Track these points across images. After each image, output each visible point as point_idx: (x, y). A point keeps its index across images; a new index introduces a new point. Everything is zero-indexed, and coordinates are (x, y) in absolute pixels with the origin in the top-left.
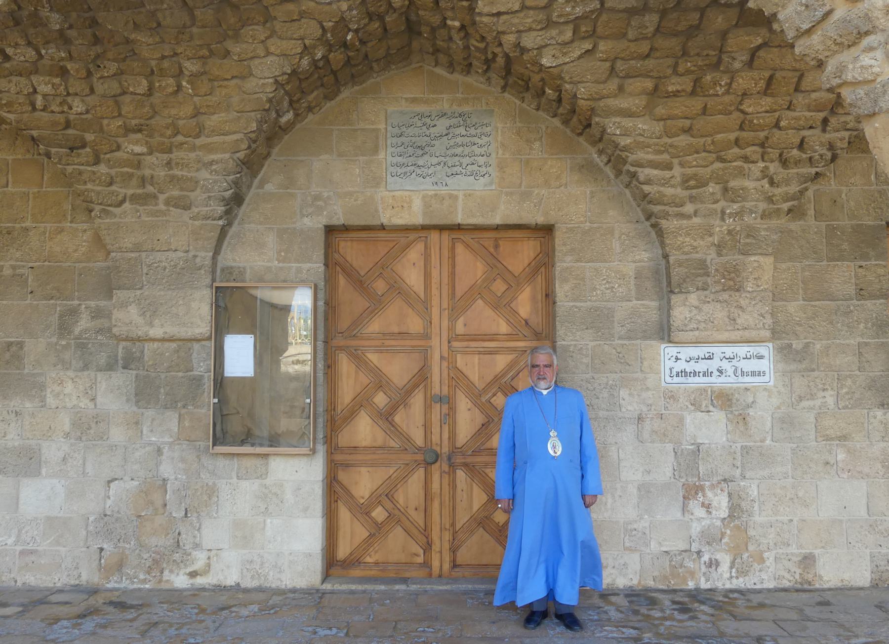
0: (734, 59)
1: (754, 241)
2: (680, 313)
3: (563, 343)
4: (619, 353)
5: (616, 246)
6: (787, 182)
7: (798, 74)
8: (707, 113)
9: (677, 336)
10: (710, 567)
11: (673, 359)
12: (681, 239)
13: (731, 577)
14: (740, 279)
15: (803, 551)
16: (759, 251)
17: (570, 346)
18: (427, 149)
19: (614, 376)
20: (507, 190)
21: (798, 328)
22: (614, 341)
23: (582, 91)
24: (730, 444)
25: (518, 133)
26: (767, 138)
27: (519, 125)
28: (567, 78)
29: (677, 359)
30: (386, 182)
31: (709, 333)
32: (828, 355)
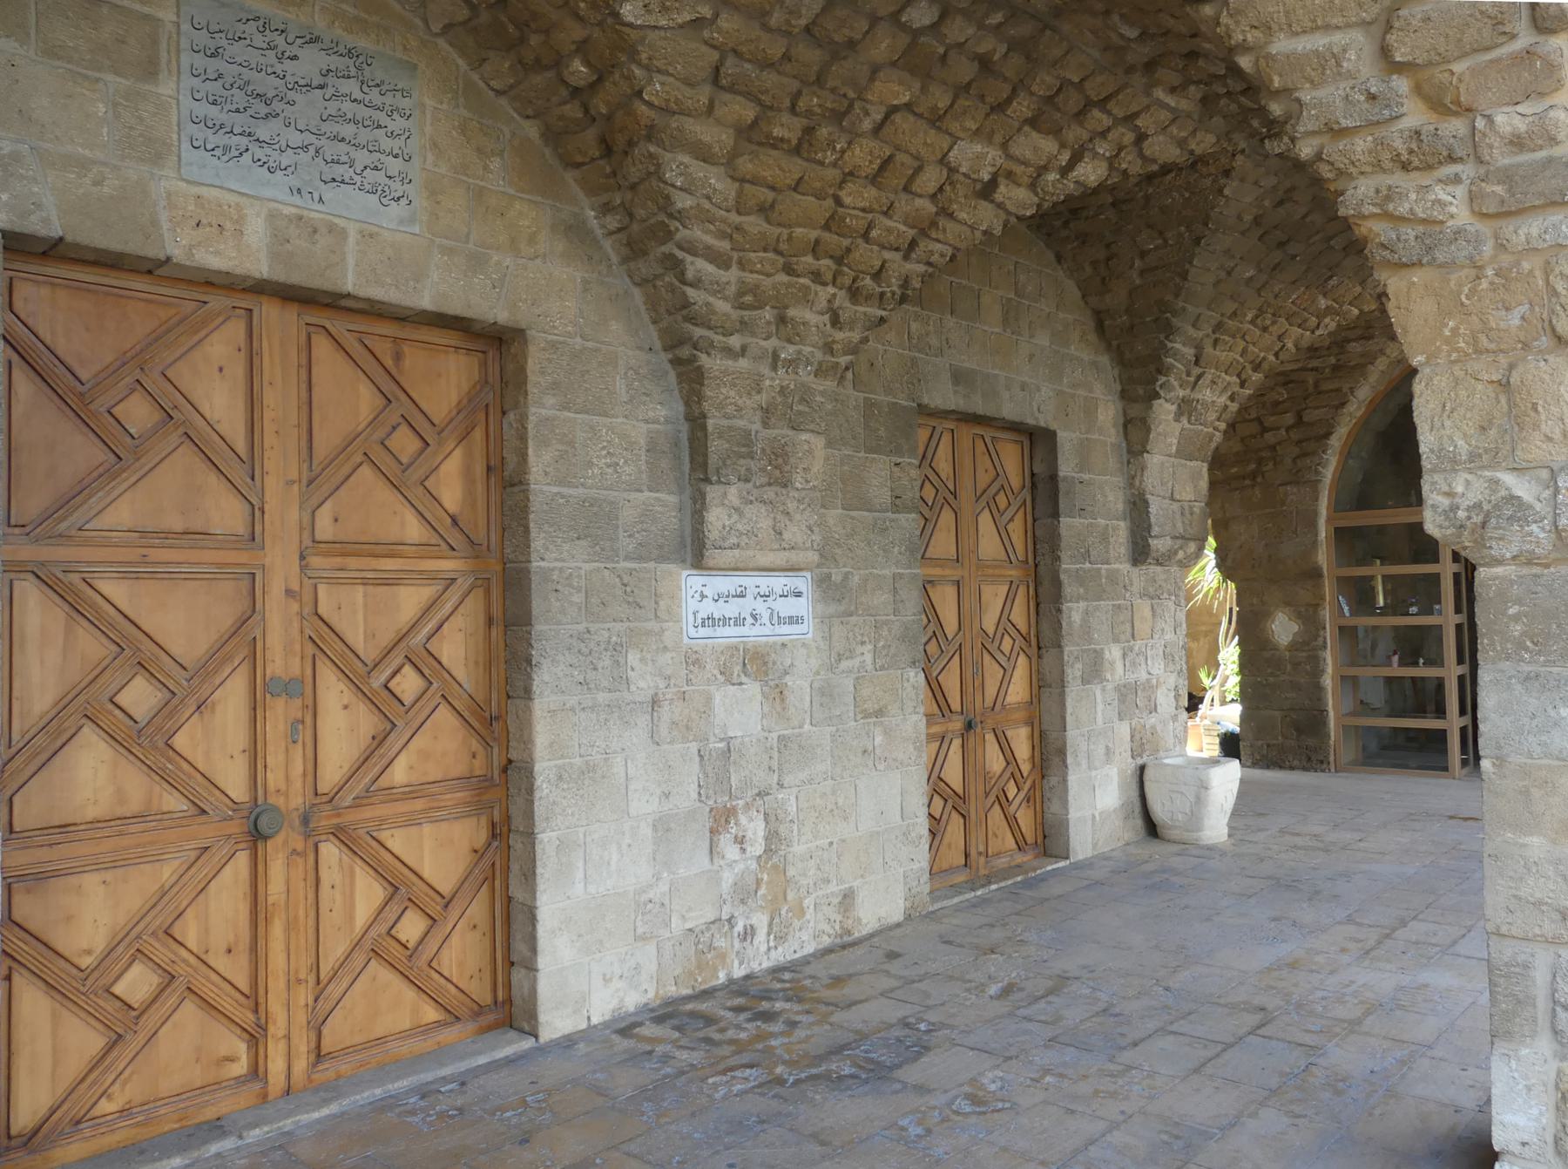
0: (867, 114)
1: (807, 409)
2: (716, 518)
3: (542, 564)
4: (626, 585)
5: (620, 386)
6: (852, 325)
7: (916, 164)
8: (800, 190)
9: (713, 556)
10: (745, 939)
11: (697, 596)
12: (724, 391)
13: (769, 949)
14: (788, 468)
15: (842, 887)
16: (812, 426)
17: (553, 570)
18: (277, 106)
19: (618, 626)
20: (445, 241)
21: (838, 551)
22: (617, 562)
23: (656, 89)
24: (766, 734)
25: (463, 129)
26: (848, 250)
27: (464, 112)
28: (644, 56)
29: (703, 596)
30: (179, 157)
31: (750, 553)
32: (866, 591)
